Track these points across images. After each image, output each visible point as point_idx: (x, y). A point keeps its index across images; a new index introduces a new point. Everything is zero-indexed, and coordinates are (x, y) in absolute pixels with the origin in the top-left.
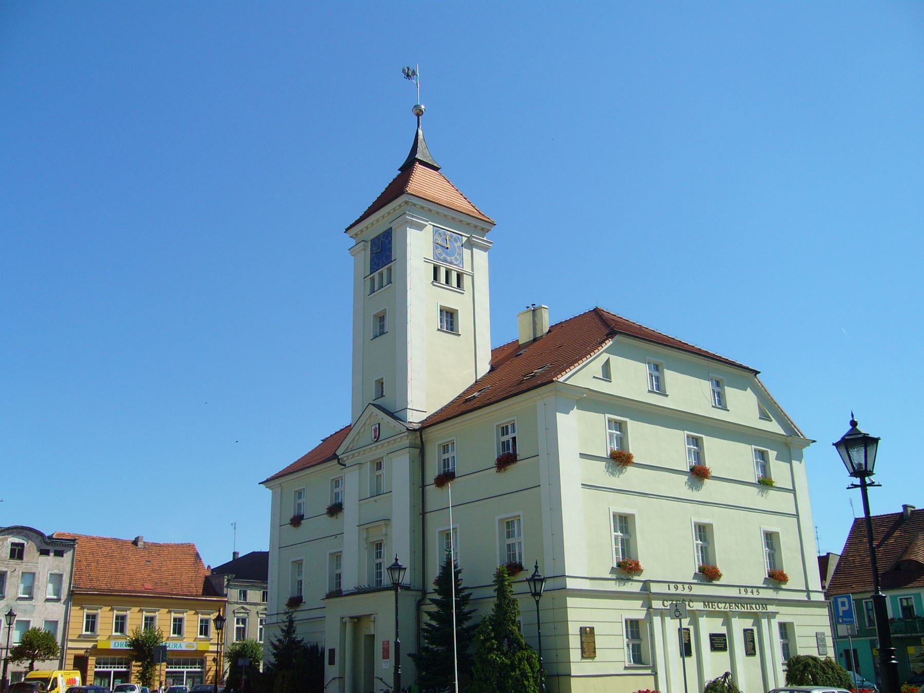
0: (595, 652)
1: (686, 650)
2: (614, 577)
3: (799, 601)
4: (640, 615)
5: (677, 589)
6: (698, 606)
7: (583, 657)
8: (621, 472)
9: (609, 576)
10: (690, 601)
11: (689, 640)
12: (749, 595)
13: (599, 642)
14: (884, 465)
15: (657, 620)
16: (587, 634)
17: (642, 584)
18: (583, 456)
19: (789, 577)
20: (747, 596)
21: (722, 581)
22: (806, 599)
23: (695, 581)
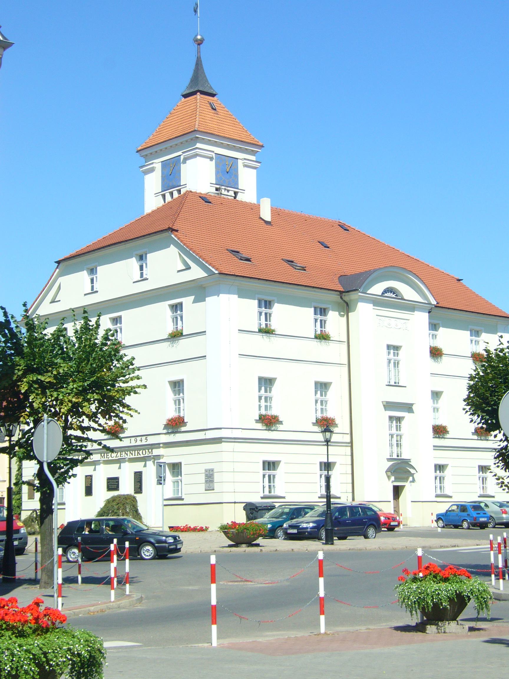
5: (141, 441)
13: (217, 477)
20: (136, 444)
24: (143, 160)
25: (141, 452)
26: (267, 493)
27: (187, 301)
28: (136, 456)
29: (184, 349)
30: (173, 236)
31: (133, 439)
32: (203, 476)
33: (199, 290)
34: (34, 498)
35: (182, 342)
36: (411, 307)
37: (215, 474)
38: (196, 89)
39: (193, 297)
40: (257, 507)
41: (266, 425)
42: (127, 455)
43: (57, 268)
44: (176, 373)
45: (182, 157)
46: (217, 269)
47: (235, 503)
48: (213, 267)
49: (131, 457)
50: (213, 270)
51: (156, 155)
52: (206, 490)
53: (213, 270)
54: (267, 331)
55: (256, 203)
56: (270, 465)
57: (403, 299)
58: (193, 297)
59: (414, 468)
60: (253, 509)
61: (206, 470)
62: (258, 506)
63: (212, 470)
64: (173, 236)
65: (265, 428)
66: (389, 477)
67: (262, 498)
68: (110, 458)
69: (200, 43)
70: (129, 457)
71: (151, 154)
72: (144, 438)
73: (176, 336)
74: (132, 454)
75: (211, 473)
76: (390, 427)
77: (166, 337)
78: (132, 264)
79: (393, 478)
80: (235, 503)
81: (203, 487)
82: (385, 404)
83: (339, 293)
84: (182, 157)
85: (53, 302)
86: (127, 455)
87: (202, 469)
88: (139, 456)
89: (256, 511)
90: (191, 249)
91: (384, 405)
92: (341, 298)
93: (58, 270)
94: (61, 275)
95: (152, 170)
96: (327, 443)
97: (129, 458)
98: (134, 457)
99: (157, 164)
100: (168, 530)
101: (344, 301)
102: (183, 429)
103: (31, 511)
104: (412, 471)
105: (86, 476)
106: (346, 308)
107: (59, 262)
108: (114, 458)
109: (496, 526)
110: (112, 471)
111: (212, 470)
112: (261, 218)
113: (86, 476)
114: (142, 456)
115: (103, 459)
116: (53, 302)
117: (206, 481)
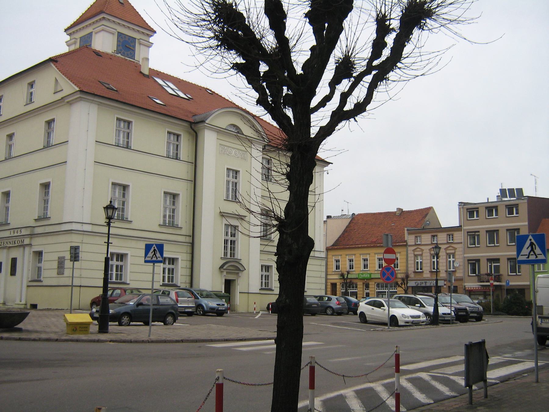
5: (17, 232)
26: (166, 282)
29: (52, 156)
31: (12, 231)
36: (250, 141)
54: (127, 147)
55: (489, 363)
57: (243, 134)
61: (59, 258)
72: (19, 230)
75: (62, 260)
76: (165, 201)
80: (80, 286)
81: (55, 271)
87: (55, 257)
92: (191, 127)
96: (110, 221)
100: (216, 306)
109: (131, 323)
112: (141, 72)
117: (58, 267)
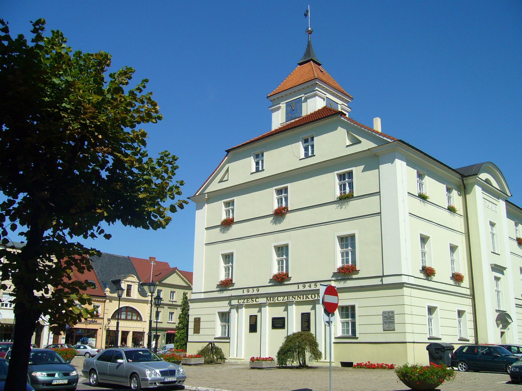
0: (199, 330)
1: (253, 328)
2: (218, 289)
3: (362, 287)
4: (227, 310)
5: (310, 286)
6: (263, 300)
7: (194, 333)
8: (228, 230)
9: (216, 289)
10: (257, 298)
11: (256, 323)
12: (307, 288)
13: (202, 325)
14: (513, 326)
15: (234, 311)
16: (197, 321)
17: (326, 287)
18: (207, 229)
19: (436, 272)
20: (305, 289)
21: (434, 278)
22: (381, 283)
23: (271, 284)
24: (271, 104)
25: (309, 296)
27: (357, 171)
28: (305, 300)
29: (353, 208)
30: (342, 118)
32: (380, 320)
33: (372, 160)
34: (199, 333)
35: (352, 203)
37: (396, 316)
38: (310, 58)
39: (362, 167)
40: (443, 347)
41: (427, 277)
42: (295, 299)
43: (226, 156)
44: (345, 229)
45: (303, 98)
46: (391, 139)
47: (414, 342)
48: (388, 138)
49: (299, 300)
50: (389, 140)
51: (283, 99)
52: (384, 330)
53: (389, 140)
56: (431, 310)
58: (362, 167)
59: (511, 319)
60: (438, 349)
62: (445, 346)
63: (393, 312)
64: (342, 118)
65: (425, 278)
66: (498, 325)
67: (429, 339)
68: (277, 301)
69: (310, 33)
70: (296, 300)
71: (278, 98)
73: (345, 198)
74: (300, 298)
75: (391, 315)
77: (336, 199)
78: (299, 147)
79: (501, 326)
80: (414, 342)
81: (380, 328)
82: (493, 266)
83: (460, 176)
84: (303, 98)
85: (221, 181)
86: (295, 299)
88: (308, 299)
89: (442, 351)
90: (363, 126)
91: (492, 267)
92: (463, 181)
93: (227, 158)
94: (228, 162)
95: (279, 108)
97: (296, 302)
98: (302, 300)
99: (283, 105)
101: (464, 183)
102: (354, 276)
103: (208, 343)
104: (510, 321)
105: (251, 316)
106: (464, 190)
107: (228, 151)
108: (281, 301)
110: (279, 312)
111: (393, 312)
113: (251, 316)
114: (311, 299)
115: (269, 302)
116: (221, 181)
